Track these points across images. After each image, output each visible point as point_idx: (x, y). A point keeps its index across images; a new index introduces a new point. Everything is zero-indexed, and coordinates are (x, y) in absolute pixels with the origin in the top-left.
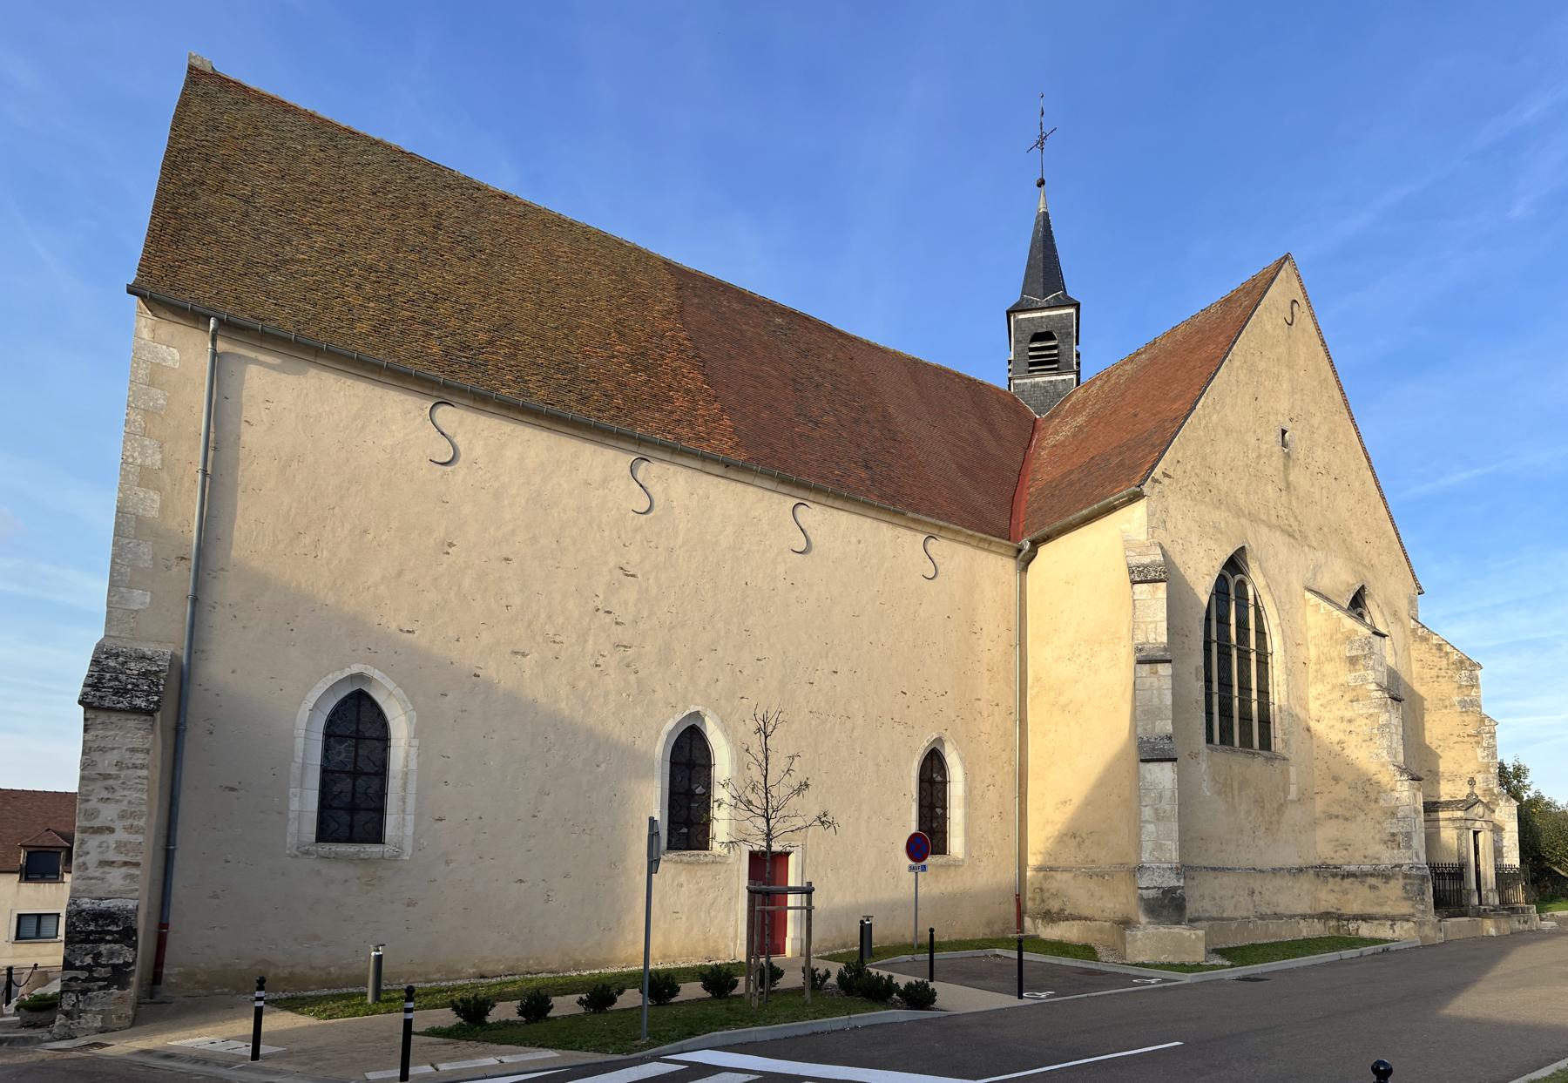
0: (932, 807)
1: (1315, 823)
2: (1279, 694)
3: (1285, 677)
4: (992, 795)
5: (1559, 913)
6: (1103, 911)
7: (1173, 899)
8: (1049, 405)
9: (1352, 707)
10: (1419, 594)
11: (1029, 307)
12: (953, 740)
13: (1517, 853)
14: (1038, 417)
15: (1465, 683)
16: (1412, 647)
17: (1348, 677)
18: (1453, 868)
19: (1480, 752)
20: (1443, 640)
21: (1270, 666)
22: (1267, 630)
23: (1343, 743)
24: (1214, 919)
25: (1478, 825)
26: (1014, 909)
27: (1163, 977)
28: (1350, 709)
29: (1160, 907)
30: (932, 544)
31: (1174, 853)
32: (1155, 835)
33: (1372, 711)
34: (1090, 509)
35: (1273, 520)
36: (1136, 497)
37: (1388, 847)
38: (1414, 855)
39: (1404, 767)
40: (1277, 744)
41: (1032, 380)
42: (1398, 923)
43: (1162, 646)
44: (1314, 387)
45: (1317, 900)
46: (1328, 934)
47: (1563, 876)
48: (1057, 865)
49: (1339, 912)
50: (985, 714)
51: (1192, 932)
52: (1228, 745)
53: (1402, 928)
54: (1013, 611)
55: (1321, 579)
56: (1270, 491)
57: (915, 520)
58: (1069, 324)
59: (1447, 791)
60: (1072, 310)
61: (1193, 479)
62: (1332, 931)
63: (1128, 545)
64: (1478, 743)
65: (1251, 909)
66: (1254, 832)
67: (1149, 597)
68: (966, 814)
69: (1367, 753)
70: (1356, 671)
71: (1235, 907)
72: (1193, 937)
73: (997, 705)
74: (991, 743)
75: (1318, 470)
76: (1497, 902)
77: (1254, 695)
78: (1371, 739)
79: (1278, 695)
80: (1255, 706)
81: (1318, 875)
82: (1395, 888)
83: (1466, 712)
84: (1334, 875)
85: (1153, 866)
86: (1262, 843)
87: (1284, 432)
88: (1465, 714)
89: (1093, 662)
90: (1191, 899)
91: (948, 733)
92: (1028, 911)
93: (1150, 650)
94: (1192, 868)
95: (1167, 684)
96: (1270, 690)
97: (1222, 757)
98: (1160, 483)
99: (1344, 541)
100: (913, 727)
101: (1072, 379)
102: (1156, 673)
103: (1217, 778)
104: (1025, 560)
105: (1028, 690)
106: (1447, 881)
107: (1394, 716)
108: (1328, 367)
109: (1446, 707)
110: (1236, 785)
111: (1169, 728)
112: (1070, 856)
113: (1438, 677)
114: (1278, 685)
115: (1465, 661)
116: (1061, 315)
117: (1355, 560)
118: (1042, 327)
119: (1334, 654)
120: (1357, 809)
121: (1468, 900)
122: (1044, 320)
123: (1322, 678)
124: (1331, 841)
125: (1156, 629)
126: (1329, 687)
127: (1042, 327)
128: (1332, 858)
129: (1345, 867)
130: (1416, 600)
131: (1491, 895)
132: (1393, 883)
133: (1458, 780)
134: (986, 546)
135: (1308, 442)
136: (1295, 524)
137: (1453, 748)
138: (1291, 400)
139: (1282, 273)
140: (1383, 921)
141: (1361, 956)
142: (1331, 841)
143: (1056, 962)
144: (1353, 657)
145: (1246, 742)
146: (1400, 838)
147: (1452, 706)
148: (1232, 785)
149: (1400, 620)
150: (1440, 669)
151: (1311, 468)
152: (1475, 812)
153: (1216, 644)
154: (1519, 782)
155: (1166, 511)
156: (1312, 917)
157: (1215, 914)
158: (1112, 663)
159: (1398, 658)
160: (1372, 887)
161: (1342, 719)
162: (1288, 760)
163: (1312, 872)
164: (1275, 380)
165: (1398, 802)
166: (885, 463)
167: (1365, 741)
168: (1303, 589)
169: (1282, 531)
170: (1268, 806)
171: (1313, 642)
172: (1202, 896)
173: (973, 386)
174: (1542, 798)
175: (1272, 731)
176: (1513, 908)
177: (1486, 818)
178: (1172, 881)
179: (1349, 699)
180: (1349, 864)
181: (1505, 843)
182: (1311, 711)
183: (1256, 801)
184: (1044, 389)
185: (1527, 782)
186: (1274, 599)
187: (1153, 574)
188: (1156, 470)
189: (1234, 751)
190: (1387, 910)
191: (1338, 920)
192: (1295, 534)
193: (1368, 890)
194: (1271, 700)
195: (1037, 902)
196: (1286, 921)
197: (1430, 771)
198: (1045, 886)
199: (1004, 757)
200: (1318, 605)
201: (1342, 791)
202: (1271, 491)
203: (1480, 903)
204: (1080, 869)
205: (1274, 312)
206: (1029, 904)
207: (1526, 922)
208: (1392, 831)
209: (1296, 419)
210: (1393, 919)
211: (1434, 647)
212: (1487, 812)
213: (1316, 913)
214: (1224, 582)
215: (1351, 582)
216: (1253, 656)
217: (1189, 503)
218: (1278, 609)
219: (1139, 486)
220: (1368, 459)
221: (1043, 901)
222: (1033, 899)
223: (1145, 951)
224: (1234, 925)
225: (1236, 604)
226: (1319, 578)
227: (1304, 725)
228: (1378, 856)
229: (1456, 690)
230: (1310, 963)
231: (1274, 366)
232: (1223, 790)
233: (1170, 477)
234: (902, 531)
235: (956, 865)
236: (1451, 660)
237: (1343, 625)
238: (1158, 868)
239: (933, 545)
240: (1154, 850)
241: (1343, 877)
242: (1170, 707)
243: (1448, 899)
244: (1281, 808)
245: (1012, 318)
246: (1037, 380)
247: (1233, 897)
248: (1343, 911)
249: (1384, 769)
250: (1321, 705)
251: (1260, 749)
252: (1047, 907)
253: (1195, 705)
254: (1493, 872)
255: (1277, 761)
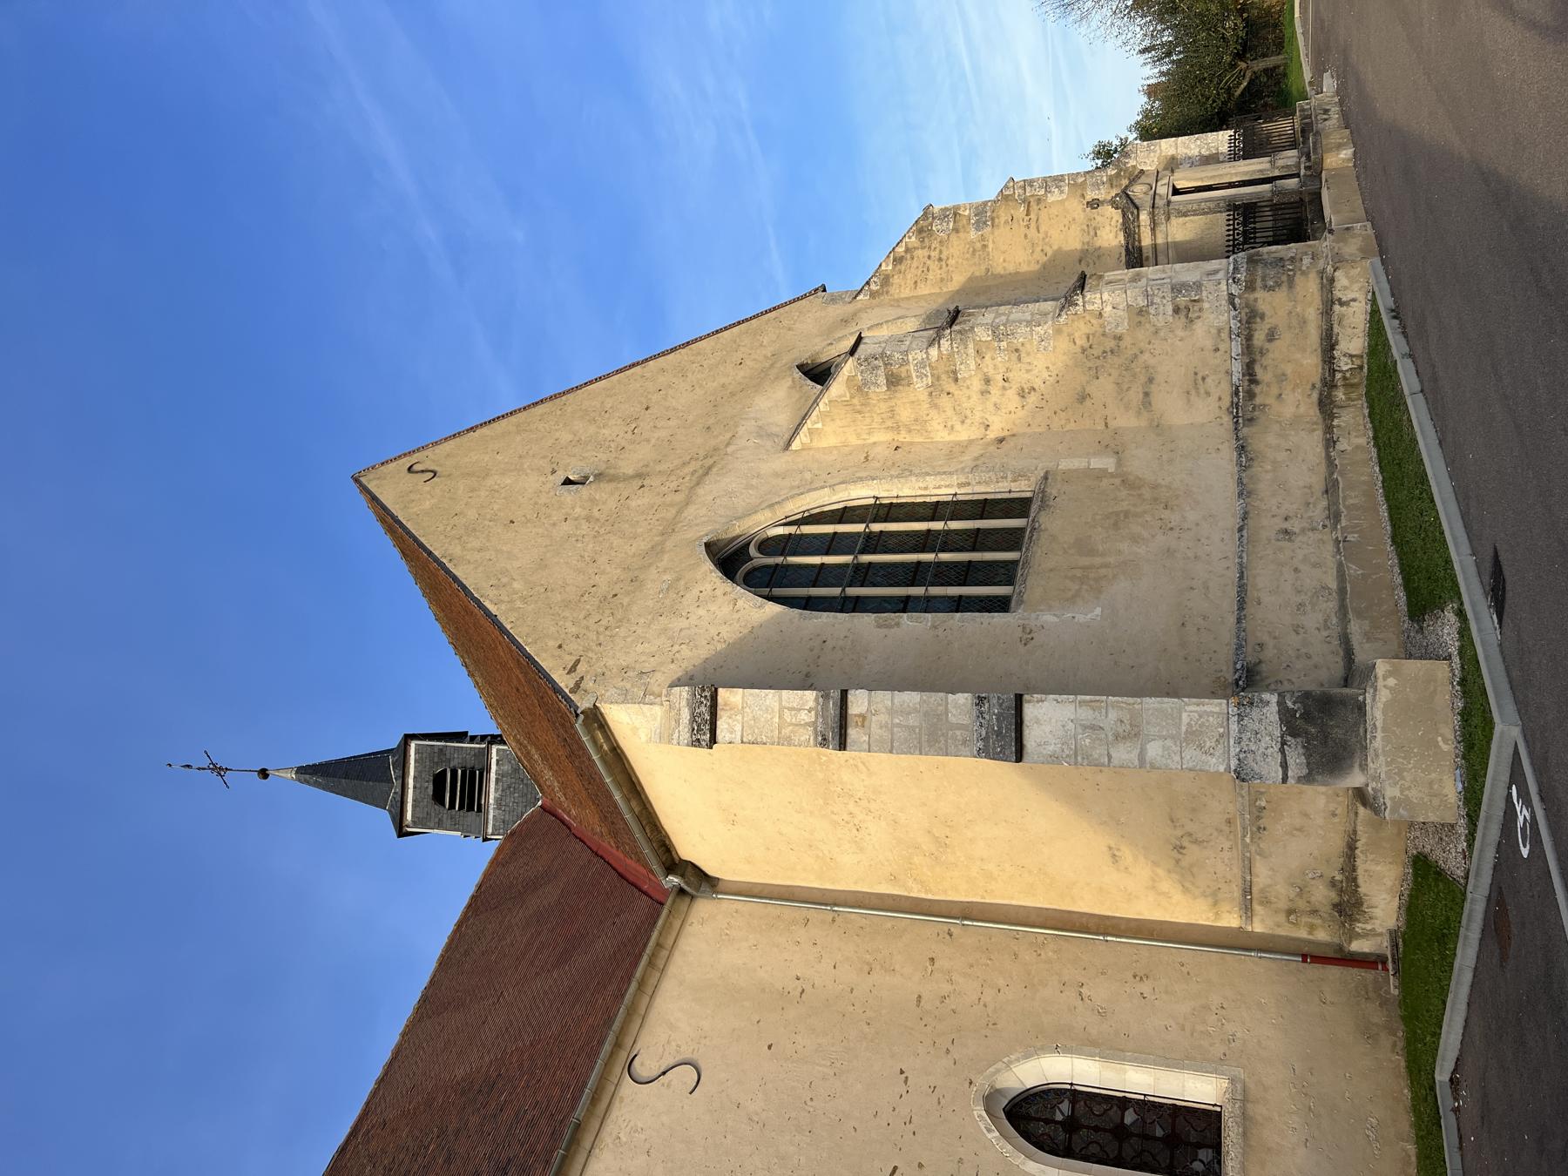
0: (1120, 1132)
1: (1157, 427)
2: (939, 487)
3: (914, 479)
4: (1100, 992)
5: (1307, 75)
6: (1334, 815)
7: (1306, 716)
8: (526, 785)
9: (964, 379)
10: (824, 290)
11: (399, 804)
12: (992, 1069)
13: (1211, 136)
14: (540, 803)
15: (951, 225)
16: (896, 296)
17: (920, 386)
18: (1234, 219)
19: (1051, 199)
20: (888, 257)
21: (895, 501)
22: (841, 506)
23: (1023, 389)
24: (1343, 610)
25: (1163, 190)
26: (1334, 971)
27: (1505, 777)
28: (968, 382)
29: (1325, 743)
30: (642, 1064)
31: (1208, 708)
32: (1169, 743)
33: (971, 351)
34: (612, 788)
35: (679, 497)
36: (595, 719)
37: (1199, 317)
38: (1211, 277)
39: (1063, 300)
40: (1021, 488)
41: (491, 807)
42: (1338, 294)
43: (821, 700)
44: (523, 439)
45: (1297, 419)
46: (1363, 402)
47: (1249, 83)
48: (1240, 881)
49: (1318, 385)
50: (946, 988)
51: (1380, 683)
52: (1015, 570)
53: (1346, 288)
54: (778, 911)
55: (778, 426)
56: (639, 502)
57: (595, 1100)
58: (429, 749)
59: (1112, 236)
60: (413, 745)
61: (592, 621)
62: (1353, 396)
63: (666, 737)
64: (1039, 201)
65: (1317, 536)
66: (1171, 529)
67: (739, 717)
68: (1134, 1060)
69: (1039, 355)
70: (909, 376)
71: (1315, 565)
72: (1391, 682)
73: (932, 959)
74: (1001, 982)
75: (630, 433)
76: (1294, 153)
77: (937, 526)
78: (1017, 350)
79: (940, 489)
80: (955, 525)
81: (1251, 420)
82: (1272, 304)
83: (993, 219)
84: (1251, 395)
85: (1234, 750)
86: (1192, 516)
87: (568, 482)
88: (997, 220)
89: (860, 794)
90: (1304, 651)
91: (979, 1080)
92: (1336, 940)
93: (825, 723)
94: (1239, 647)
95: (883, 698)
96: (935, 499)
97: (1034, 585)
98: (582, 678)
99: (733, 394)
100: (961, 1161)
101: (498, 750)
102: (863, 717)
103: (1070, 594)
104: (700, 881)
105: (912, 895)
106: (1258, 225)
107: (980, 319)
108: (504, 422)
109: (985, 246)
110: (1085, 561)
111: (963, 699)
112: (1221, 861)
113: (940, 259)
114: (926, 488)
115: (919, 226)
116: (416, 761)
117: (760, 381)
118: (427, 788)
119: (883, 407)
120: (1133, 365)
121: (1292, 192)
122: (418, 785)
123: (920, 423)
124: (1189, 401)
125: (793, 709)
126: (933, 413)
127: (427, 788)
128: (1220, 399)
129: (1235, 379)
130: (832, 295)
131: (1280, 163)
132: (1262, 307)
133: (1094, 224)
134: (664, 953)
135: (589, 448)
136: (693, 466)
137: (1046, 233)
138: (529, 471)
139: (370, 486)
140: (1335, 318)
141: (1410, 356)
142: (1189, 401)
143: (1468, 977)
144: (887, 381)
145: (1013, 539)
146: (1182, 300)
147: (983, 238)
148: (1084, 568)
149: (855, 314)
150: (929, 257)
151: (623, 443)
152: (1142, 196)
153: (847, 589)
154: (1116, 151)
155: (625, 670)
156: (1329, 429)
157: (1331, 605)
158: (860, 765)
159: (907, 313)
160: (1271, 337)
161: (985, 393)
162: (1047, 472)
163: (1245, 430)
164: (496, 495)
165: (1121, 307)
166: (511, 1126)
167: (1019, 360)
168: (787, 453)
169: (698, 484)
170: (1125, 506)
171: (865, 436)
172: (1297, 629)
173: (479, 905)
174: (1137, 123)
175: (999, 496)
176: (1303, 131)
177: (1152, 180)
178: (1268, 714)
179: (953, 384)
180: (1229, 373)
181: (1195, 152)
182: (973, 437)
183: (1116, 526)
184: (505, 791)
185: (1116, 142)
186: (792, 497)
187: (703, 709)
188: (562, 685)
189: (1026, 562)
190: (1312, 313)
191: (1334, 386)
192: (707, 465)
193: (1277, 343)
194: (949, 498)
195: (1318, 921)
196: (1341, 474)
197: (1080, 261)
198: (1283, 904)
199: (1027, 956)
200: (811, 431)
201: (1103, 388)
202: (641, 500)
203: (1297, 175)
204: (1245, 846)
205: (412, 496)
206: (1322, 935)
207: (1326, 111)
208: (1170, 312)
209: (554, 466)
210: (1329, 304)
211: (898, 267)
212: (1143, 179)
213: (1320, 421)
214: (756, 573)
215: (790, 383)
216: (877, 527)
217: (622, 632)
218: (809, 491)
219: (577, 715)
220: (633, 365)
221: (1314, 912)
222: (1312, 928)
223: (1431, 783)
224: (1353, 570)
225: (794, 554)
226: (775, 429)
227: (992, 448)
228: (1214, 331)
229: (961, 234)
230: (1437, 452)
231: (479, 496)
232: (1092, 582)
233: (578, 661)
234: (610, 1128)
235: (1243, 1096)
236: (917, 244)
237: (840, 396)
238: (1239, 741)
239: (644, 1067)
240: (1200, 747)
241: (1253, 380)
242: (925, 695)
243: (1289, 222)
244: (1127, 482)
245: (409, 830)
246: (491, 801)
247: (1296, 570)
248: (1316, 379)
249: (1065, 328)
250: (963, 422)
251: (1027, 517)
252: (1328, 908)
253: (940, 631)
254: (1242, 162)
255: (1048, 490)
